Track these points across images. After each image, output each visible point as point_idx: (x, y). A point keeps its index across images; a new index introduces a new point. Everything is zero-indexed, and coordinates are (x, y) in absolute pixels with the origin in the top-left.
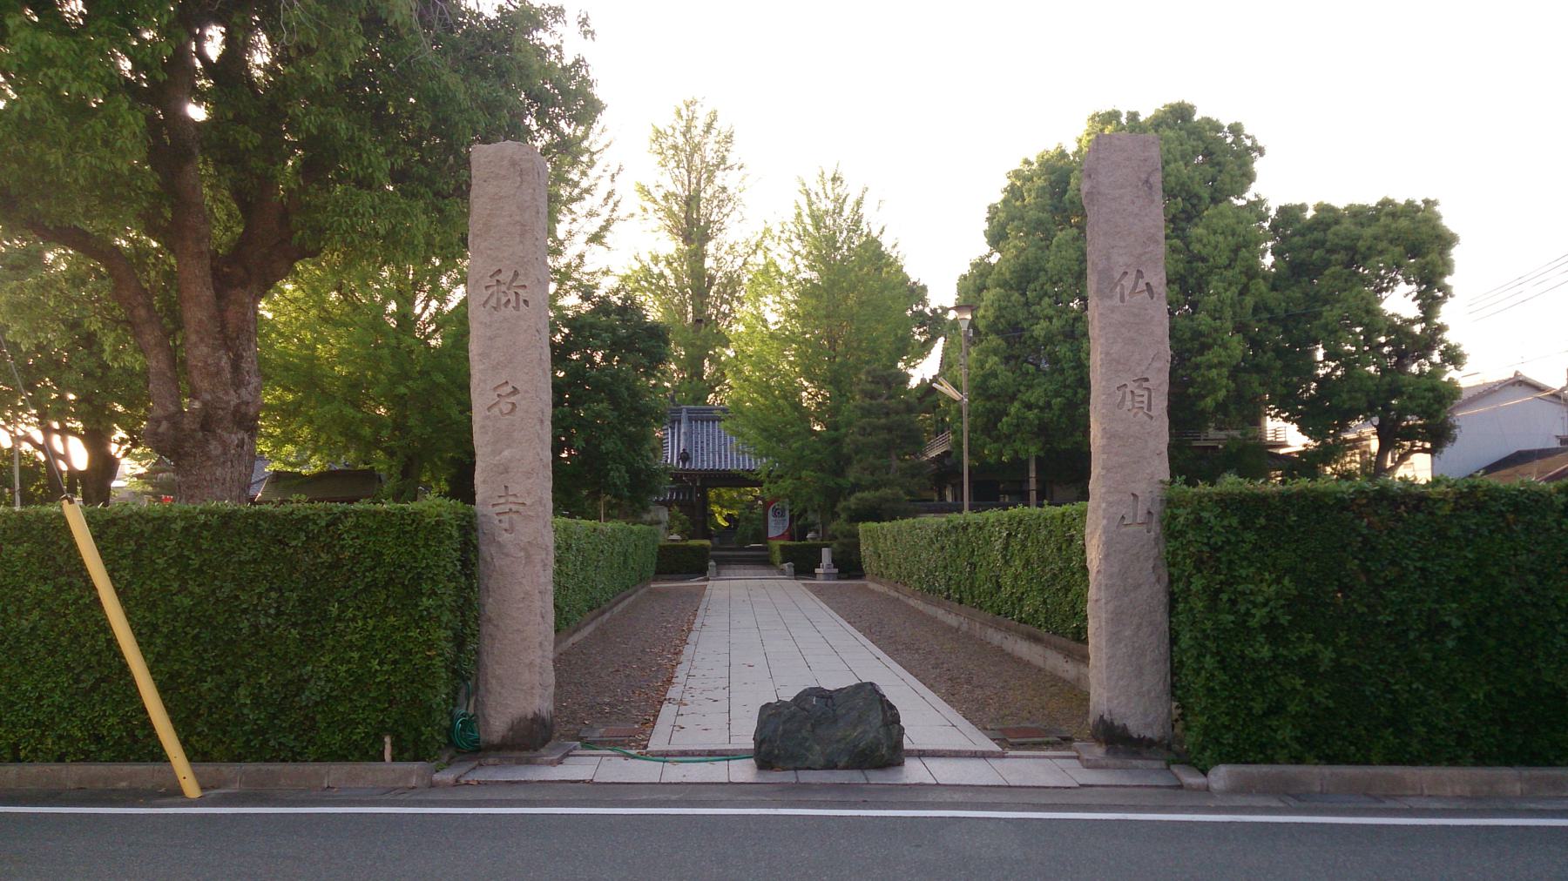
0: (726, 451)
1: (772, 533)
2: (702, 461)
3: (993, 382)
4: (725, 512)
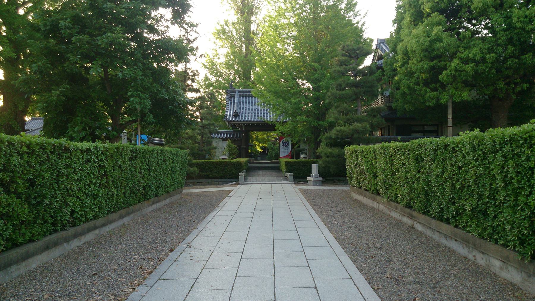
0: (258, 112)
1: (282, 154)
2: (245, 117)
3: (438, 45)
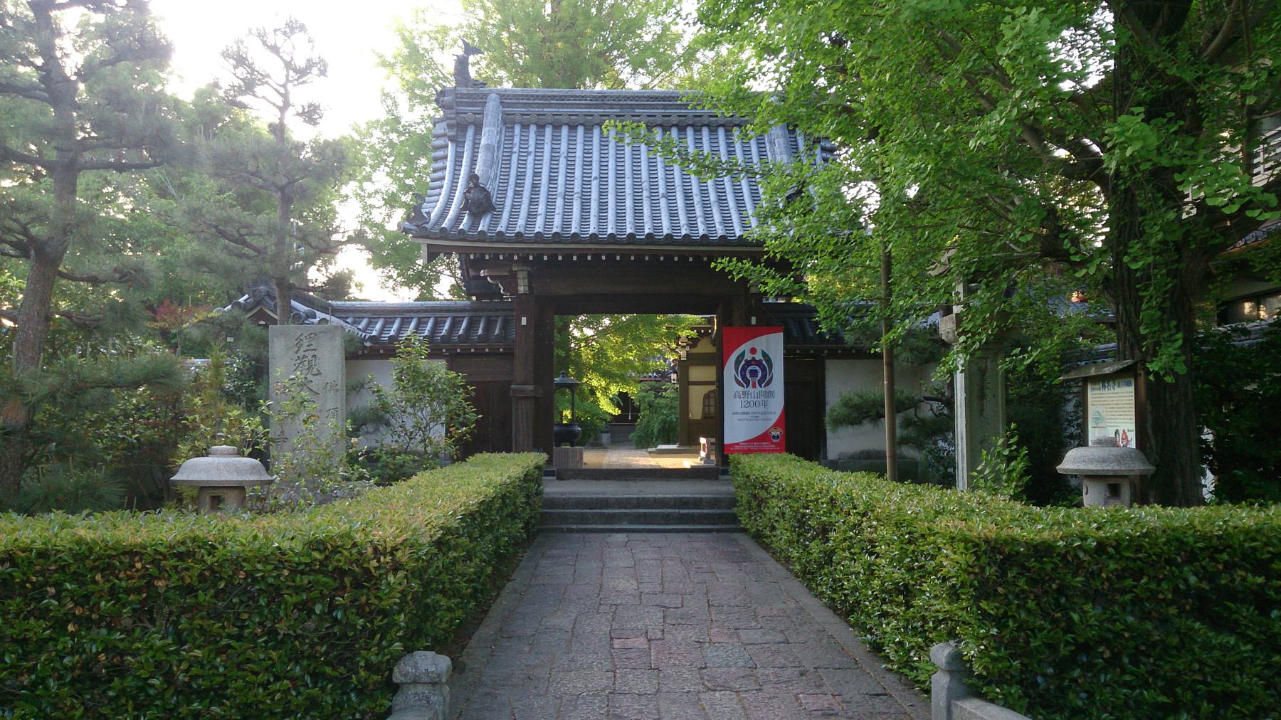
4: (614, 389)
